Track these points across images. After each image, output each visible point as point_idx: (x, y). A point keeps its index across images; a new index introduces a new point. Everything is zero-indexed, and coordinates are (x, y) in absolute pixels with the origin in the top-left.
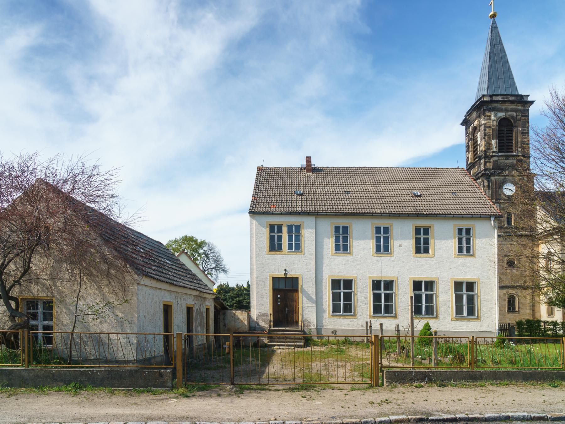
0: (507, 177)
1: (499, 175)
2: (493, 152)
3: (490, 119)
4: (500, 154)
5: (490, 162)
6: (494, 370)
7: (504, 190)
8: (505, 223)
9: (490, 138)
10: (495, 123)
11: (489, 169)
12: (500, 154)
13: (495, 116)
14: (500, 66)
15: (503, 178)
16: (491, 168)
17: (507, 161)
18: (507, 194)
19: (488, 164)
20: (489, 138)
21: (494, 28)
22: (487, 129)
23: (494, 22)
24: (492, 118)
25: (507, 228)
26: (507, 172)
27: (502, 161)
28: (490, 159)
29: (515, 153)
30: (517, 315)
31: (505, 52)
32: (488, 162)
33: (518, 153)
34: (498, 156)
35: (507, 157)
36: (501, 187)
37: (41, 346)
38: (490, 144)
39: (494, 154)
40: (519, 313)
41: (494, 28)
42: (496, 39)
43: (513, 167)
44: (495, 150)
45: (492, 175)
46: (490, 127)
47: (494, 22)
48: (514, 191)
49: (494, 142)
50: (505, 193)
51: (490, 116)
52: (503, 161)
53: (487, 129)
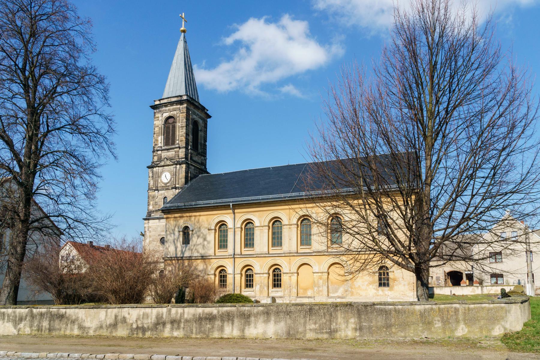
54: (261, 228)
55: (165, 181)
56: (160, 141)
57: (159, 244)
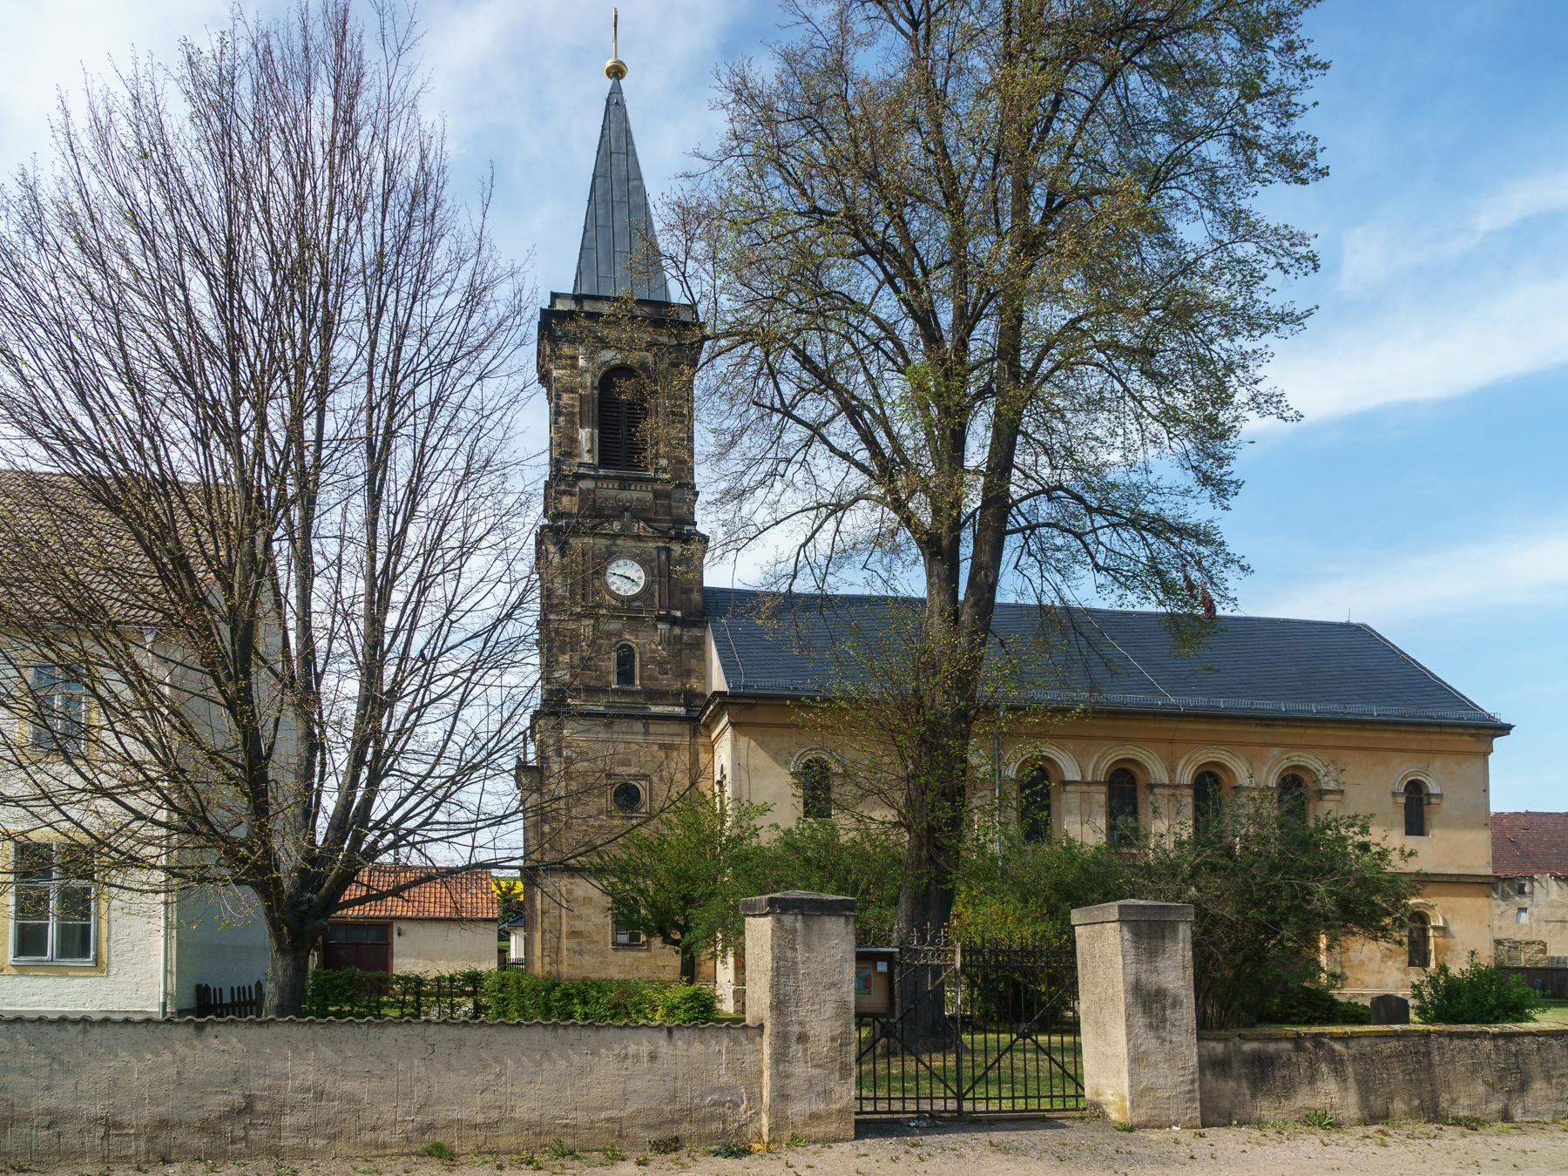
0: (619, 542)
1: (593, 532)
2: (581, 465)
3: (574, 366)
4: (601, 472)
5: (572, 494)
6: (1189, 946)
7: (611, 580)
8: (613, 678)
9: (573, 423)
10: (588, 378)
11: (569, 515)
12: (601, 472)
13: (589, 359)
14: (621, 216)
15: (605, 542)
16: (575, 510)
17: (625, 495)
18: (622, 593)
19: (565, 500)
20: (571, 422)
21: (615, 106)
22: (565, 396)
23: (616, 91)
24: (581, 362)
25: (615, 691)
26: (617, 526)
27: (610, 491)
28: (574, 485)
29: (651, 473)
30: (642, 955)
31: (640, 178)
32: (564, 493)
33: (656, 471)
34: (596, 478)
35: (624, 484)
36: (600, 573)
37: (768, 618)
38: (574, 441)
39: (582, 470)
40: (648, 950)
41: (615, 106)
42: (618, 138)
43: (639, 513)
44: (587, 458)
45: (576, 532)
46: (572, 390)
47: (616, 91)
48: (642, 583)
49: (584, 434)
50: (613, 588)
51: (574, 358)
52: (612, 493)
53: (565, 396)
54: (1085, 788)
57: (606, 801)
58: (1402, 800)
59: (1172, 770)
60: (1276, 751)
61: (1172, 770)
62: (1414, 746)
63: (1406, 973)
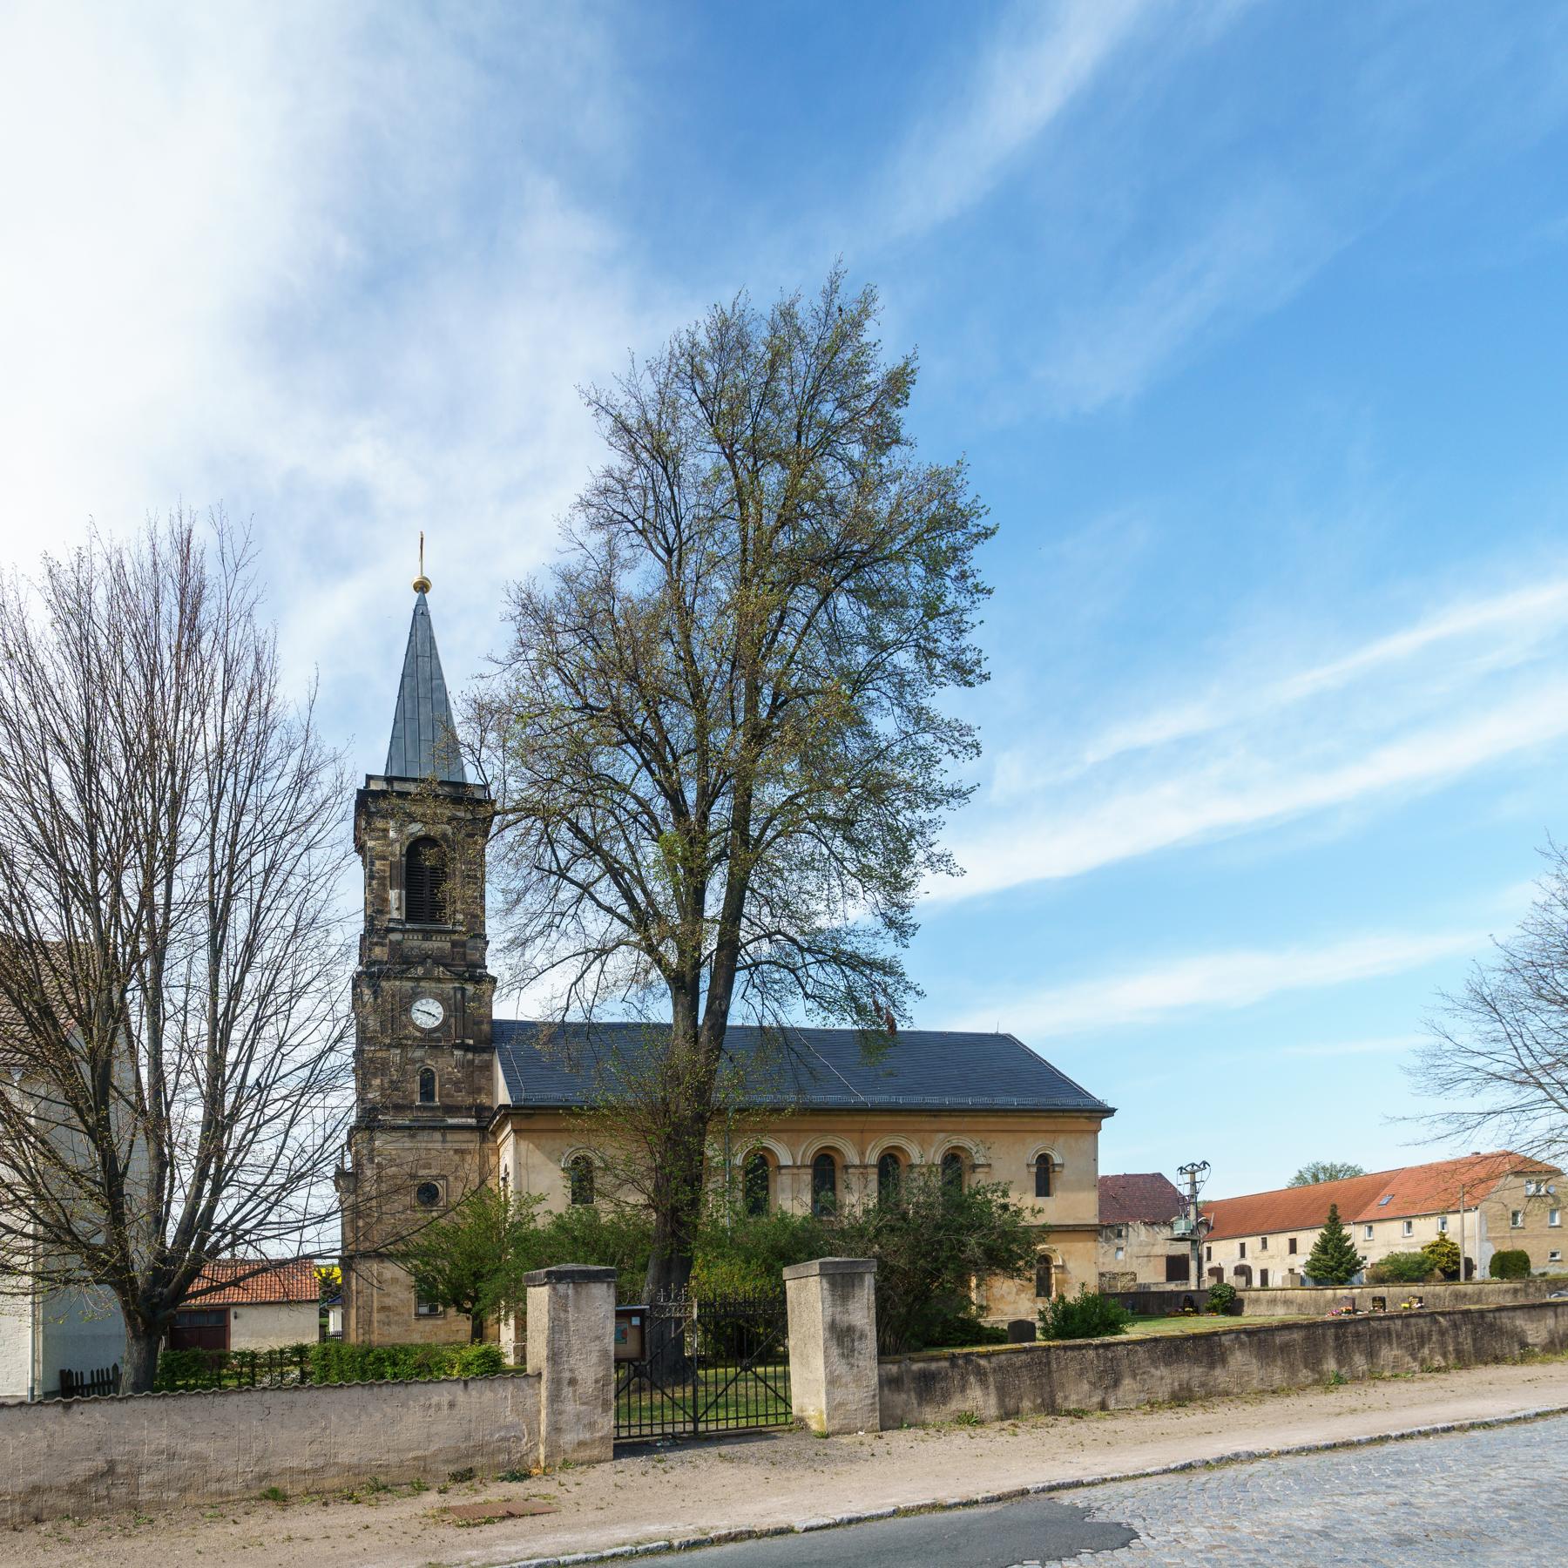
2: (390, 920)
39: (392, 925)
55: (428, 1023)
56: (394, 903)
57: (409, 1199)
58: (1034, 1170)
59: (862, 1154)
60: (942, 1135)
61: (862, 1154)
62: (1044, 1128)
63: (1034, 1302)
